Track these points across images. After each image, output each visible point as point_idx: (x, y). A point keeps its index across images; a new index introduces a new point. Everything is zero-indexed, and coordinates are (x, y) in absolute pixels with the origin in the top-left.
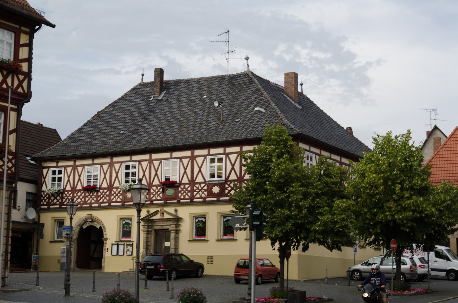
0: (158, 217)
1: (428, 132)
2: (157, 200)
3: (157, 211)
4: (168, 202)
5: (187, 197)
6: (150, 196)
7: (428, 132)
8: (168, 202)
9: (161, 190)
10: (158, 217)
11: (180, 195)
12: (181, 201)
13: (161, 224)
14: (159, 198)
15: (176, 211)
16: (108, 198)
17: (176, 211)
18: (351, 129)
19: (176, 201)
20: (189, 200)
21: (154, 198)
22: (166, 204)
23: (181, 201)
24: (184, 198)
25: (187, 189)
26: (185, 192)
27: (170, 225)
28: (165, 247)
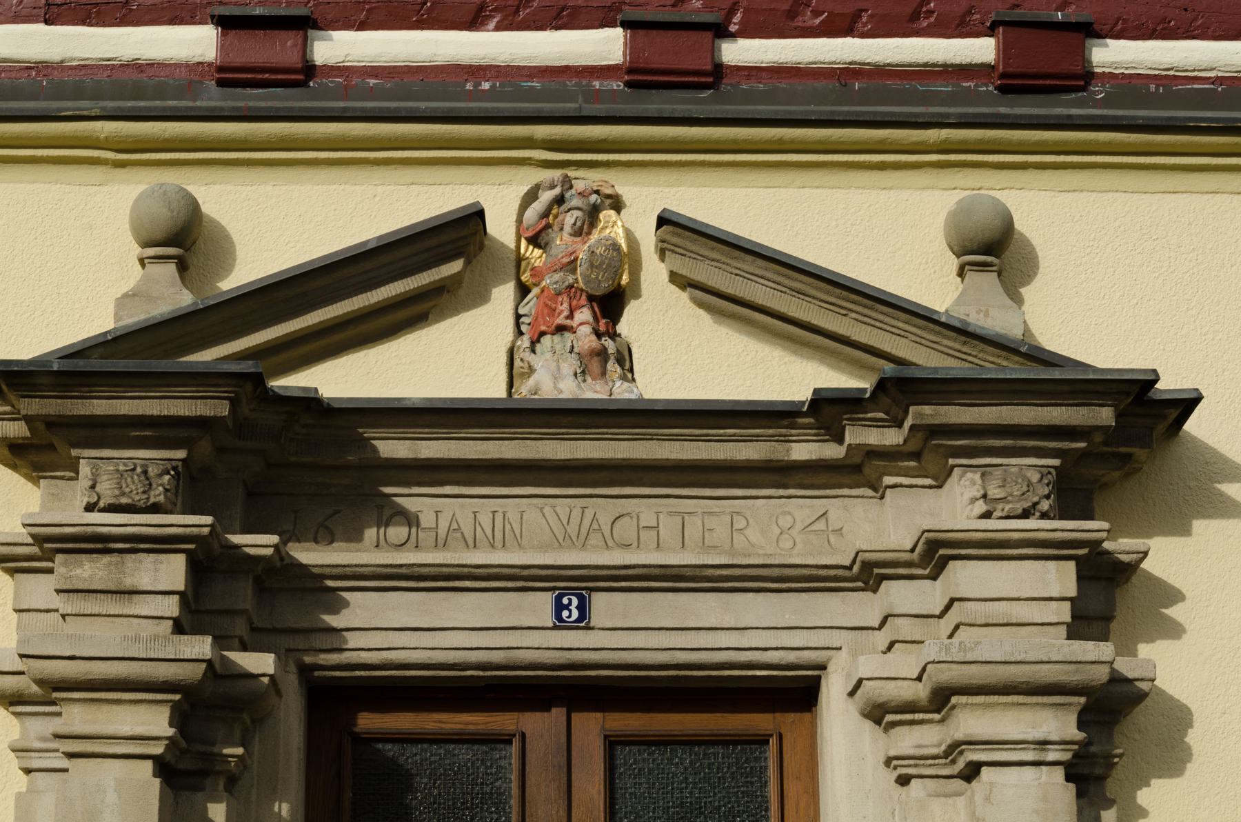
0: (456, 357)
4: (740, 51)
8: (740, 51)
10: (456, 357)
13: (539, 527)
15: (992, 250)
17: (992, 250)
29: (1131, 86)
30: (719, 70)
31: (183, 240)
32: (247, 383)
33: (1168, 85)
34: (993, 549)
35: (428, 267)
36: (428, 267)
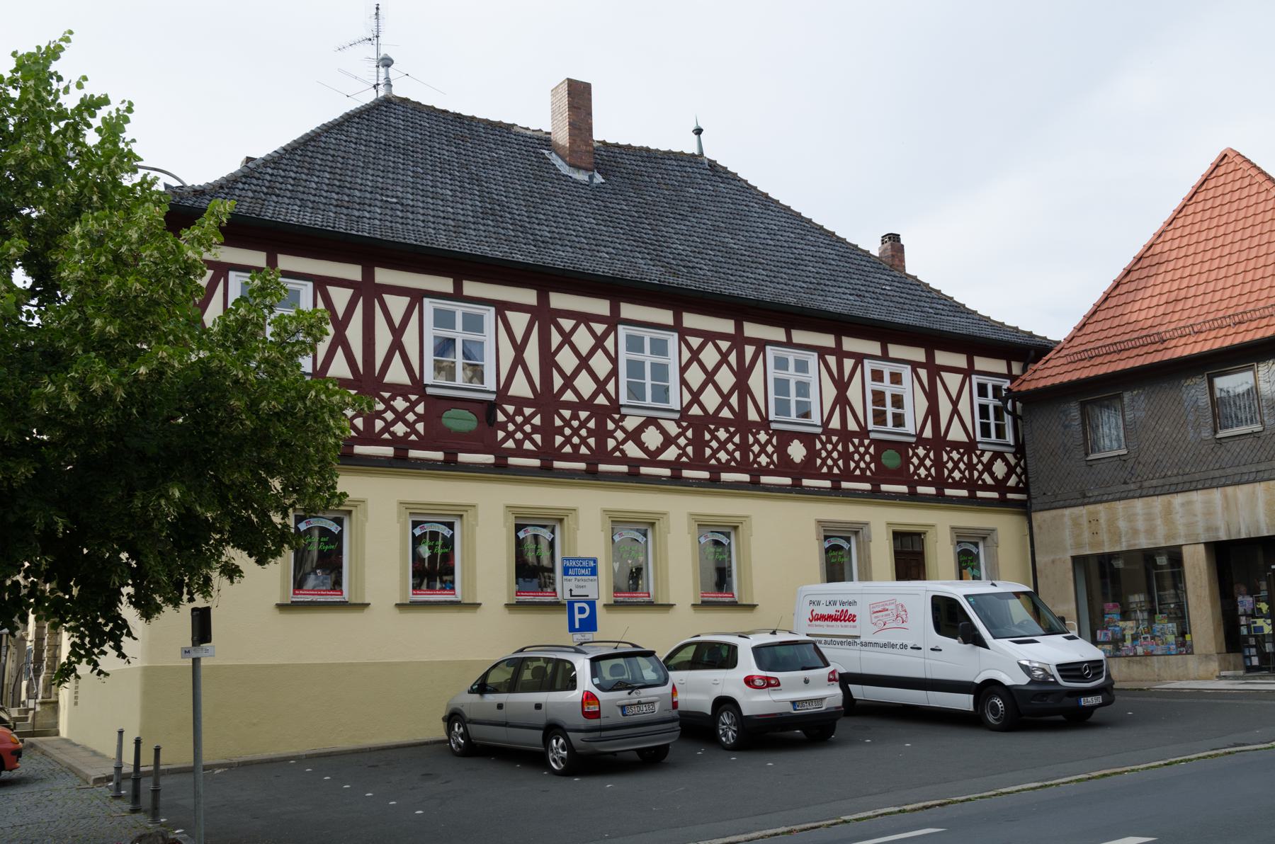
20: (536, 462)
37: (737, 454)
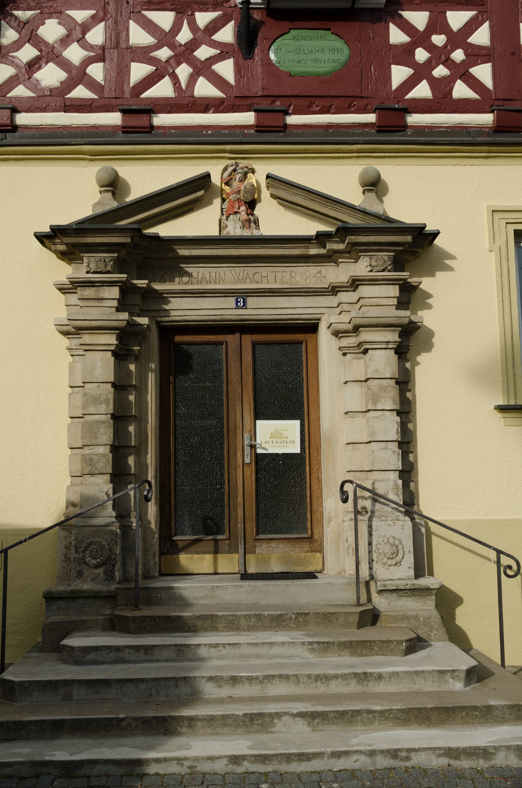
0: (202, 222)
1: (457, 601)
2: (186, 103)
3: (204, 180)
4: (293, 120)
5: (461, 90)
6: (123, 72)
7: (457, 601)
8: (293, 120)
9: (227, 34)
10: (202, 222)
11: (399, 74)
12: (414, 119)
13: (230, 277)
14: (204, 88)
15: (374, 185)
16: (484, 72)
17: (374, 185)
18: (51, 226)
19: (371, 118)
21: (163, 89)
22: (272, 133)
23: (414, 119)
24: (442, 101)
25: (459, 39)
26: (440, 56)
27: (355, 283)
28: (259, 459)
29: (420, 130)
30: (286, 126)
31: (113, 185)
32: (136, 231)
33: (432, 129)
34: (373, 282)
35: (192, 194)
36: (192, 194)
37: (96, 71)
